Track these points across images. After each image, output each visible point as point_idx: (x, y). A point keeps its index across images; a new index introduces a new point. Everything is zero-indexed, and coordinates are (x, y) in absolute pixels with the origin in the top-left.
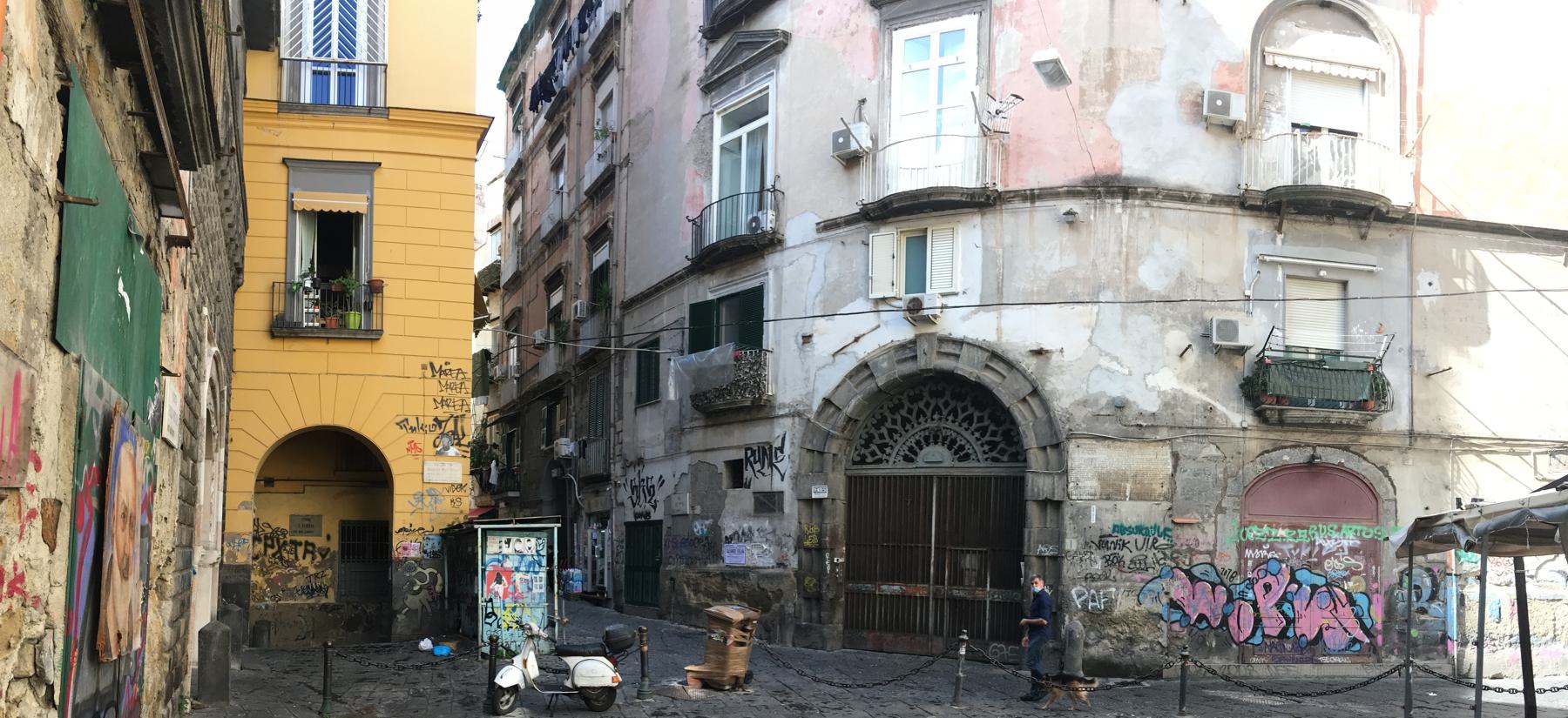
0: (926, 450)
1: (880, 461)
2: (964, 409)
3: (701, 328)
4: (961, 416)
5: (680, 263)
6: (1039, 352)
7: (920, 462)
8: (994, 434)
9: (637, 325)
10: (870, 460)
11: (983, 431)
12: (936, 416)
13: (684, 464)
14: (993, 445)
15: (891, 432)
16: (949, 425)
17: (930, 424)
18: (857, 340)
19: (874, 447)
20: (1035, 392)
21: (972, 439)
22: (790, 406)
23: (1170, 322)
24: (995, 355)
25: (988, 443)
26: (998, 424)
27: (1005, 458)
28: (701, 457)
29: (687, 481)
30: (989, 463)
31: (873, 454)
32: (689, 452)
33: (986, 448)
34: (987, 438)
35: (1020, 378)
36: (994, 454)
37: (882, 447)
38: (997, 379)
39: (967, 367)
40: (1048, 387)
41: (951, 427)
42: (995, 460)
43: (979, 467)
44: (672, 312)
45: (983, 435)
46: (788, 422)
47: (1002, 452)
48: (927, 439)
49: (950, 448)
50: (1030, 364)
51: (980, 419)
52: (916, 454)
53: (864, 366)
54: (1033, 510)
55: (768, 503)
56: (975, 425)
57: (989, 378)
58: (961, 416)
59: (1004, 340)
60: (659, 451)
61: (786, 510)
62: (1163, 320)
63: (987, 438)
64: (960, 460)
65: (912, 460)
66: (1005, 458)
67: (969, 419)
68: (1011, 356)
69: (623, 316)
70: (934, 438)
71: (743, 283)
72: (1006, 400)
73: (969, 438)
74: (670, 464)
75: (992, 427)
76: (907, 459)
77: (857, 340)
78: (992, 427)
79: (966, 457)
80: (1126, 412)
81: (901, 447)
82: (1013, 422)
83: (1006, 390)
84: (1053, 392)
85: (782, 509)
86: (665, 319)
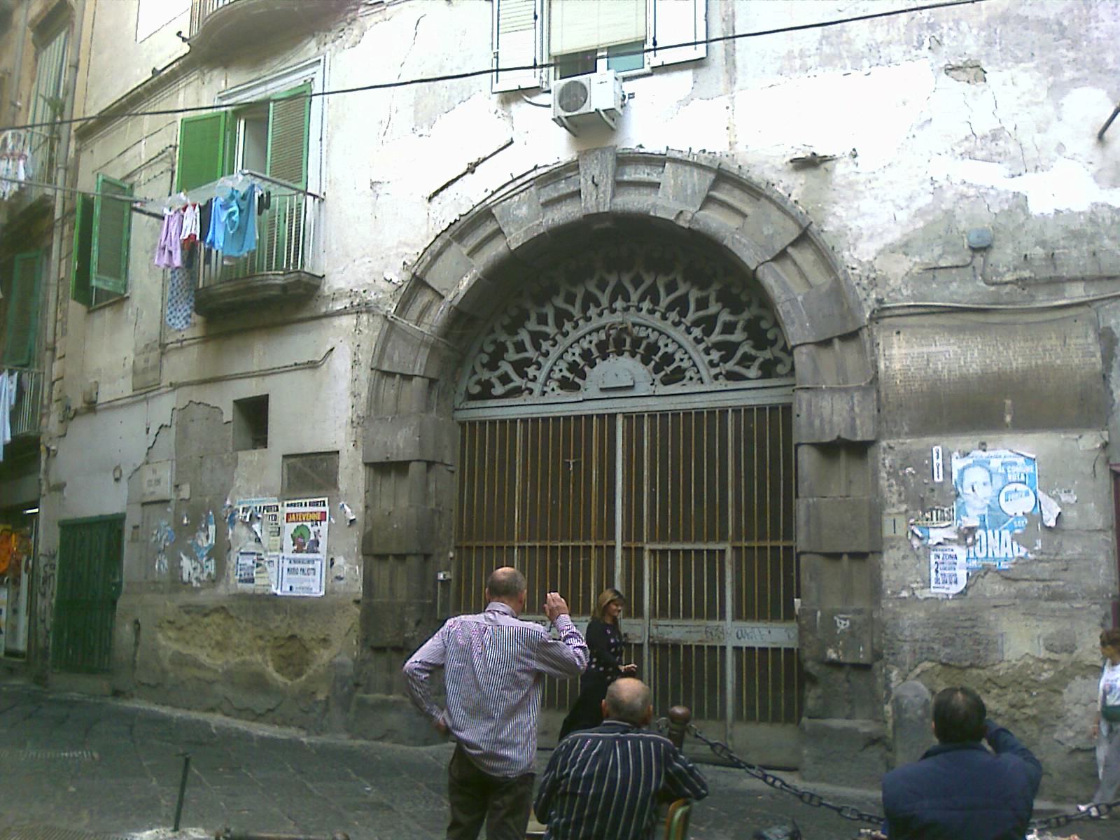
0: (601, 366)
1: (518, 391)
2: (671, 288)
3: (200, 156)
4: (665, 301)
5: (171, 49)
6: (809, 163)
7: (591, 386)
8: (729, 328)
9: (97, 166)
10: (499, 389)
11: (708, 324)
12: (619, 304)
13: (163, 408)
14: (728, 350)
15: (537, 338)
16: (644, 318)
17: (608, 319)
18: (471, 169)
19: (505, 367)
20: (805, 237)
21: (687, 341)
22: (352, 293)
23: (1068, 74)
24: (724, 178)
25: (718, 346)
26: (736, 309)
27: (753, 372)
28: (197, 394)
29: (169, 437)
30: (722, 384)
31: (505, 379)
32: (174, 386)
33: (715, 355)
34: (716, 337)
35: (775, 214)
36: (730, 366)
37: (521, 367)
38: (733, 222)
39: (670, 200)
40: (830, 226)
41: (643, 318)
42: (732, 376)
43: (705, 392)
44: (150, 142)
45: (708, 332)
46: (348, 322)
47: (747, 360)
48: (603, 348)
49: (646, 361)
50: (794, 187)
51: (702, 304)
52: (583, 376)
53: (483, 214)
54: (807, 460)
55: (310, 473)
56: (692, 316)
57: (716, 221)
58: (665, 301)
59: (740, 148)
60: (124, 387)
61: (343, 483)
62: (1055, 69)
63: (716, 337)
64: (667, 381)
65: (577, 387)
66: (753, 372)
67: (681, 305)
68: (756, 176)
69: (78, 151)
70: (617, 343)
71: (275, 84)
72: (750, 257)
73: (680, 339)
74: (140, 409)
75: (725, 317)
76: (565, 384)
77: (471, 169)
78: (725, 317)
79: (677, 376)
80: (994, 256)
81: (554, 360)
82: (766, 302)
83: (745, 236)
84: (841, 233)
85: (335, 484)
86: (144, 151)
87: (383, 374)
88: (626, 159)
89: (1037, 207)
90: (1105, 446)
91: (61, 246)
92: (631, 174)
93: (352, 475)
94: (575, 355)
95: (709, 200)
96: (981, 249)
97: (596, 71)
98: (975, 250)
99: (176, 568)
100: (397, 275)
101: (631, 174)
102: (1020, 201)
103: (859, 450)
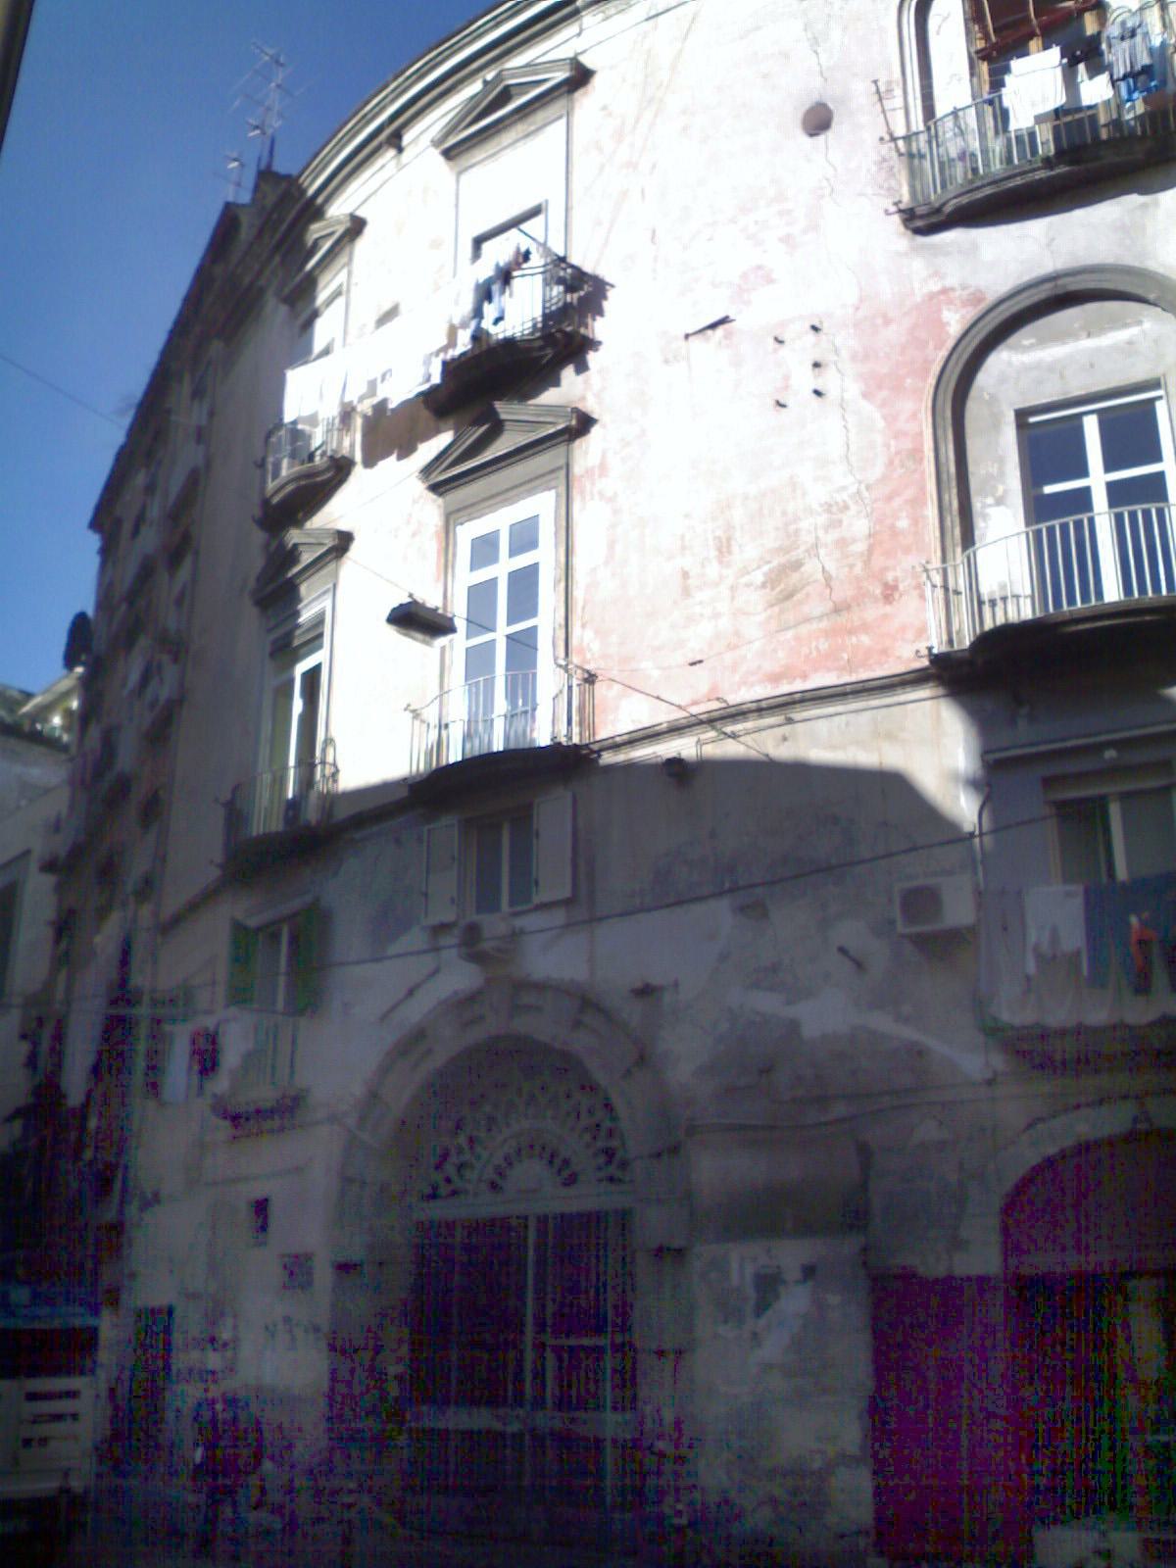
6: (645, 991)
18: (411, 993)
53: (419, 1035)
57: (580, 1043)
77: (411, 993)
79: (571, 1180)
87: (347, 1180)
88: (522, 985)
89: (810, 1030)
90: (865, 1249)
91: (438, 119)
92: (527, 998)
93: (323, 1275)
94: (498, 1159)
95: (577, 1024)
96: (766, 1070)
97: (467, 650)
98: (761, 1072)
99: (1071, 1288)
100: (358, 1090)
101: (527, 998)
102: (794, 1026)
103: (679, 1253)
